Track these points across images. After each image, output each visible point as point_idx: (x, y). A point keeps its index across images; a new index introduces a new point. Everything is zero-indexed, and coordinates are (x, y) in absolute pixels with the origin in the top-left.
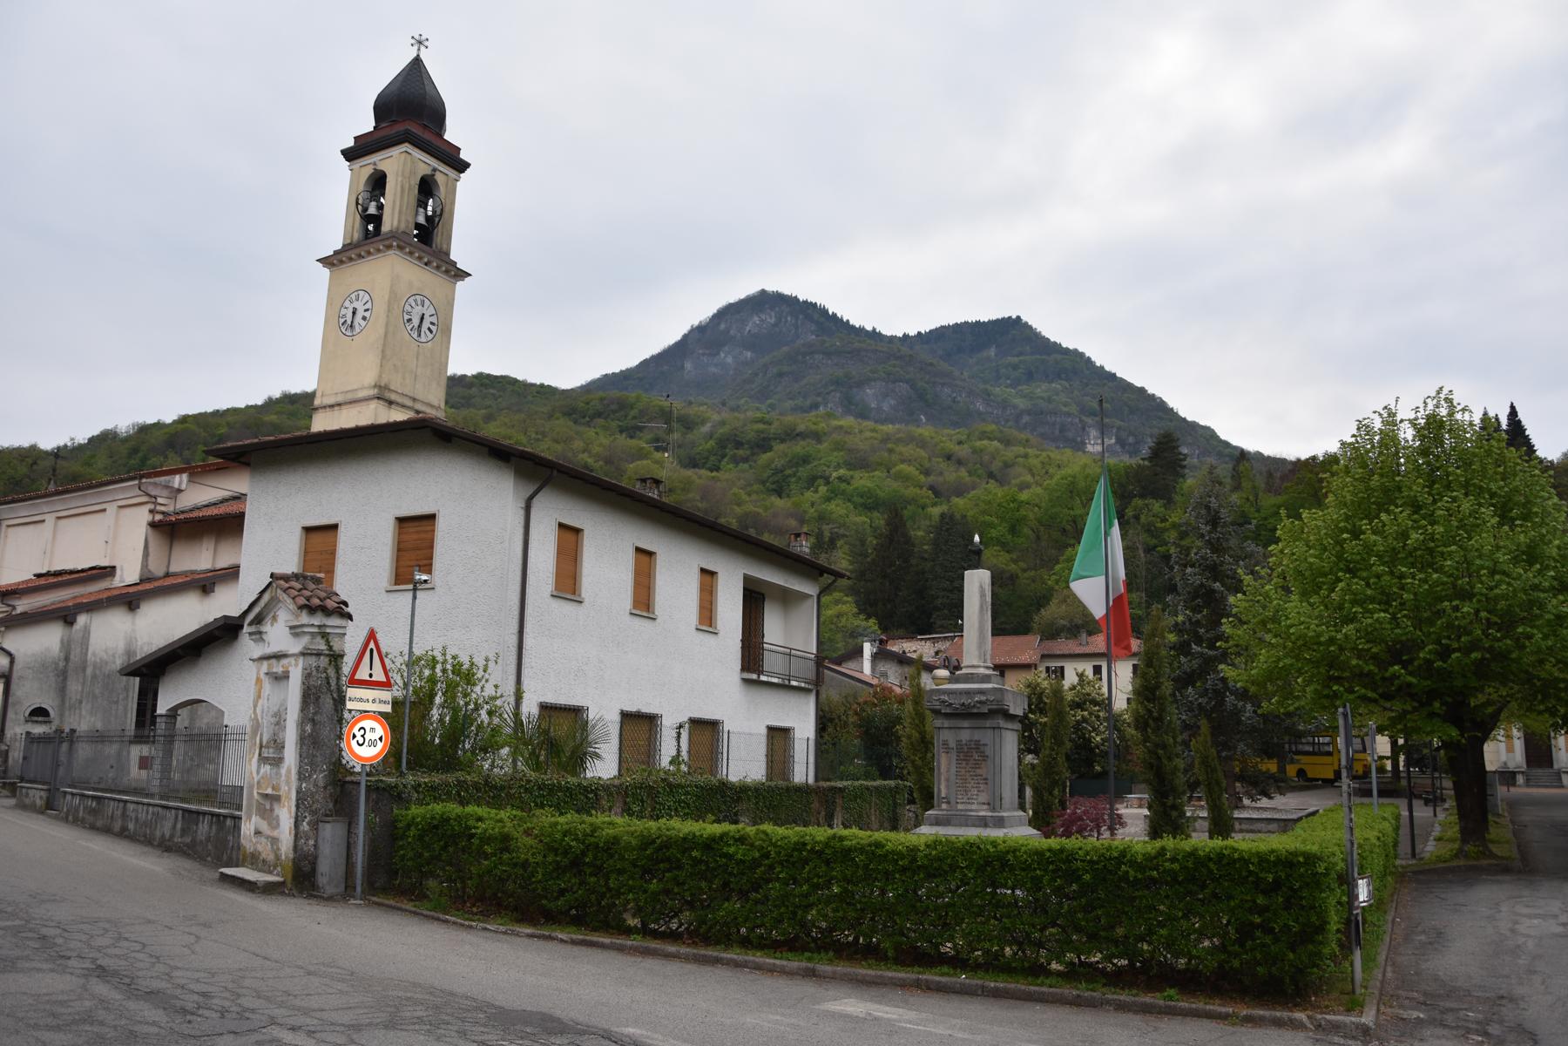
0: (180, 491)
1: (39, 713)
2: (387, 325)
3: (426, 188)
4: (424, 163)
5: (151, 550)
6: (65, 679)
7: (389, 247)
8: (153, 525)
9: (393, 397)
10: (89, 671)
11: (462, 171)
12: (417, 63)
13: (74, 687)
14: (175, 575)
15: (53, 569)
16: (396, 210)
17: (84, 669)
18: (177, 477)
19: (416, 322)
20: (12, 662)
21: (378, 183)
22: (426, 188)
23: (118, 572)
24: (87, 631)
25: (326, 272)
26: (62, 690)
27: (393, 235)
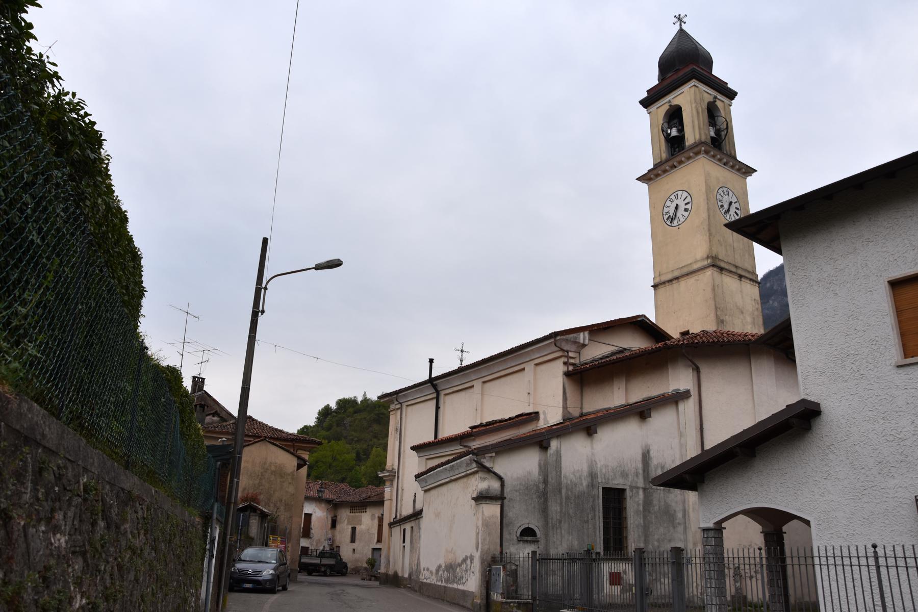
0: (584, 345)
1: (528, 533)
2: (708, 210)
3: (712, 112)
4: (708, 94)
5: (568, 395)
6: (546, 500)
7: (697, 154)
8: (567, 374)
9: (722, 265)
10: (564, 491)
11: (732, 99)
12: (681, 31)
13: (554, 508)
14: (587, 414)
15: (484, 422)
16: (694, 130)
17: (560, 492)
18: (582, 334)
19: (726, 207)
20: (503, 485)
21: (675, 116)
22: (712, 112)
23: (542, 416)
24: (558, 454)
25: (645, 186)
26: (544, 511)
27: (692, 147)
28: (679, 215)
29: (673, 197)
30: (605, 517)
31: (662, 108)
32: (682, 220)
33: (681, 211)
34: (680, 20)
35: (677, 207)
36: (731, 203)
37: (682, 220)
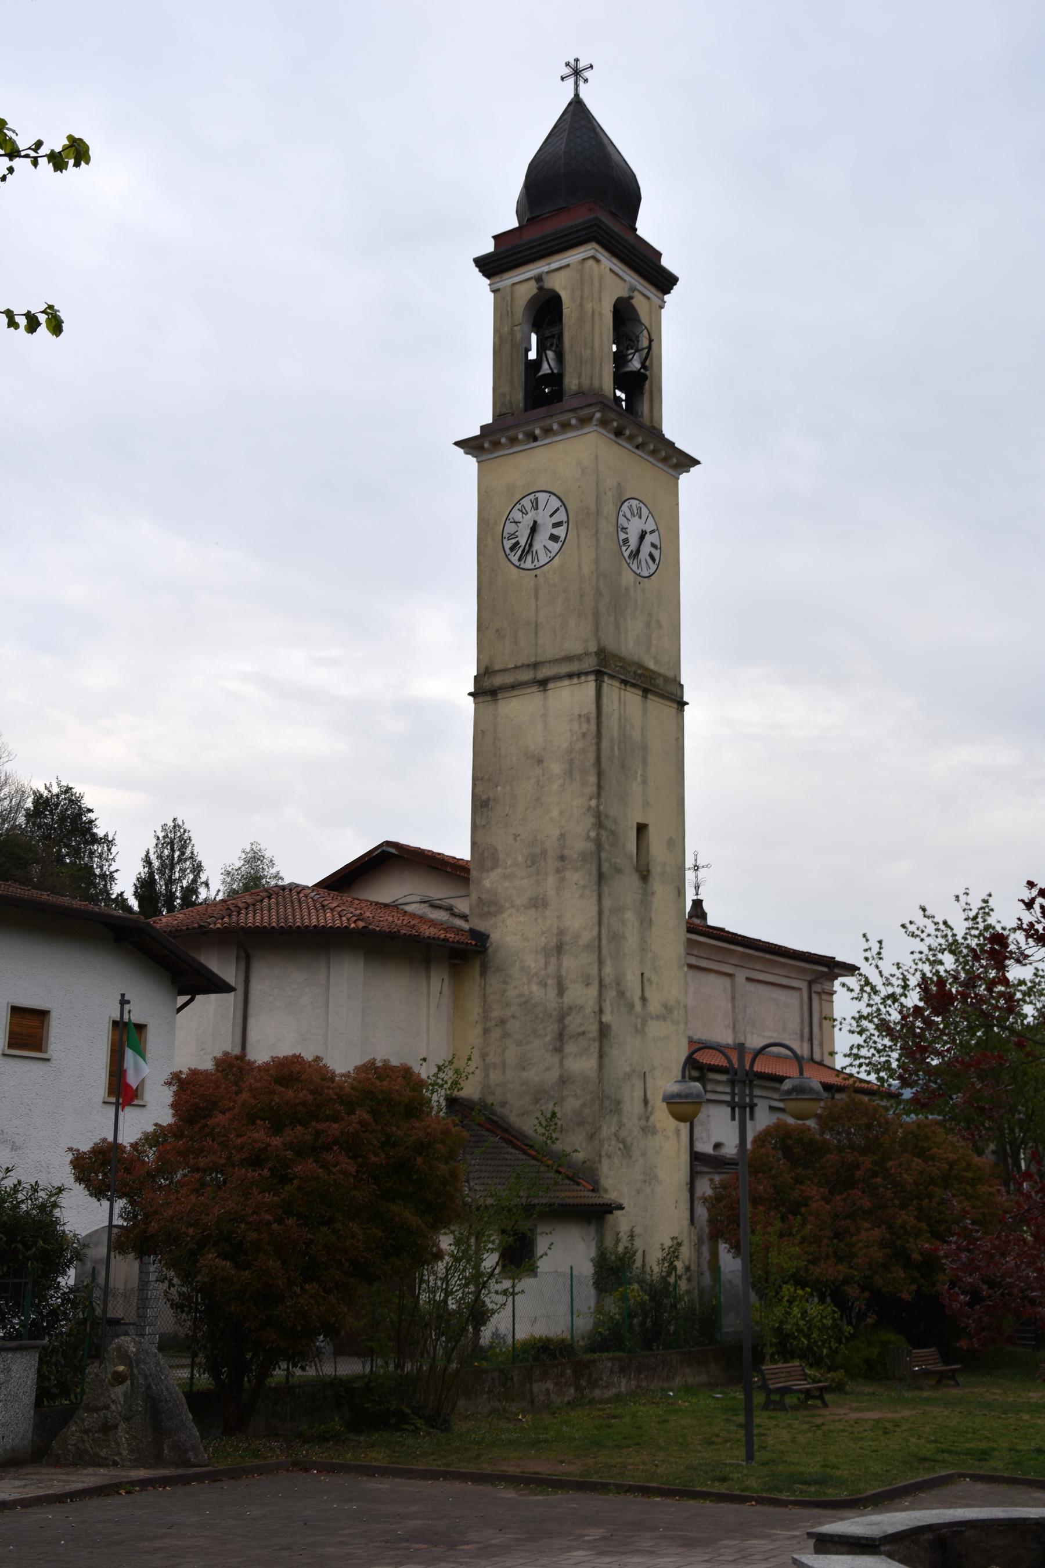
7: (584, 421)
11: (667, 290)
12: (577, 109)
21: (546, 313)
25: (471, 463)
28: (538, 546)
29: (526, 502)
30: (1016, 1506)
31: (522, 281)
32: (543, 559)
33: (541, 541)
34: (577, 73)
35: (534, 529)
36: (642, 536)
37: (543, 559)
